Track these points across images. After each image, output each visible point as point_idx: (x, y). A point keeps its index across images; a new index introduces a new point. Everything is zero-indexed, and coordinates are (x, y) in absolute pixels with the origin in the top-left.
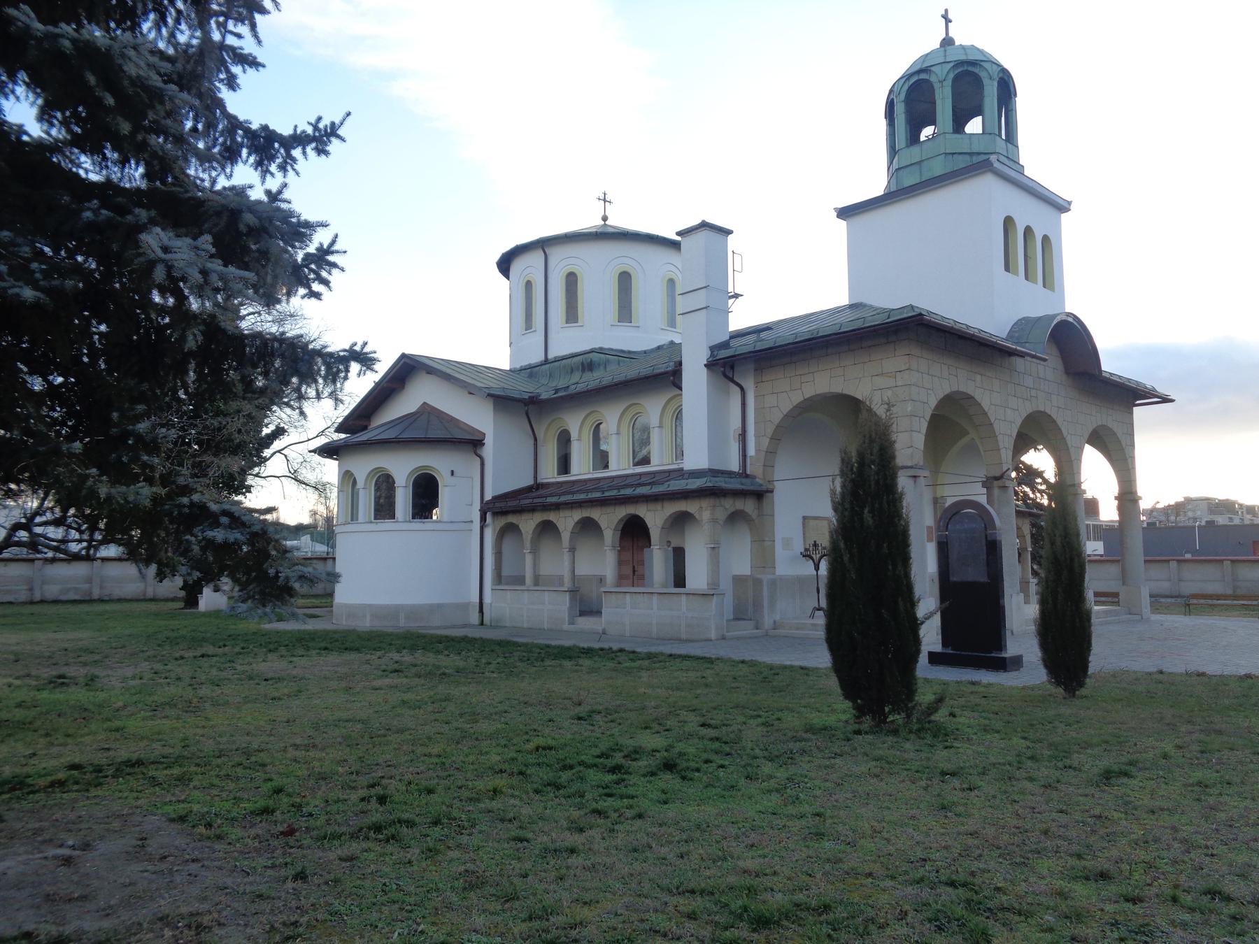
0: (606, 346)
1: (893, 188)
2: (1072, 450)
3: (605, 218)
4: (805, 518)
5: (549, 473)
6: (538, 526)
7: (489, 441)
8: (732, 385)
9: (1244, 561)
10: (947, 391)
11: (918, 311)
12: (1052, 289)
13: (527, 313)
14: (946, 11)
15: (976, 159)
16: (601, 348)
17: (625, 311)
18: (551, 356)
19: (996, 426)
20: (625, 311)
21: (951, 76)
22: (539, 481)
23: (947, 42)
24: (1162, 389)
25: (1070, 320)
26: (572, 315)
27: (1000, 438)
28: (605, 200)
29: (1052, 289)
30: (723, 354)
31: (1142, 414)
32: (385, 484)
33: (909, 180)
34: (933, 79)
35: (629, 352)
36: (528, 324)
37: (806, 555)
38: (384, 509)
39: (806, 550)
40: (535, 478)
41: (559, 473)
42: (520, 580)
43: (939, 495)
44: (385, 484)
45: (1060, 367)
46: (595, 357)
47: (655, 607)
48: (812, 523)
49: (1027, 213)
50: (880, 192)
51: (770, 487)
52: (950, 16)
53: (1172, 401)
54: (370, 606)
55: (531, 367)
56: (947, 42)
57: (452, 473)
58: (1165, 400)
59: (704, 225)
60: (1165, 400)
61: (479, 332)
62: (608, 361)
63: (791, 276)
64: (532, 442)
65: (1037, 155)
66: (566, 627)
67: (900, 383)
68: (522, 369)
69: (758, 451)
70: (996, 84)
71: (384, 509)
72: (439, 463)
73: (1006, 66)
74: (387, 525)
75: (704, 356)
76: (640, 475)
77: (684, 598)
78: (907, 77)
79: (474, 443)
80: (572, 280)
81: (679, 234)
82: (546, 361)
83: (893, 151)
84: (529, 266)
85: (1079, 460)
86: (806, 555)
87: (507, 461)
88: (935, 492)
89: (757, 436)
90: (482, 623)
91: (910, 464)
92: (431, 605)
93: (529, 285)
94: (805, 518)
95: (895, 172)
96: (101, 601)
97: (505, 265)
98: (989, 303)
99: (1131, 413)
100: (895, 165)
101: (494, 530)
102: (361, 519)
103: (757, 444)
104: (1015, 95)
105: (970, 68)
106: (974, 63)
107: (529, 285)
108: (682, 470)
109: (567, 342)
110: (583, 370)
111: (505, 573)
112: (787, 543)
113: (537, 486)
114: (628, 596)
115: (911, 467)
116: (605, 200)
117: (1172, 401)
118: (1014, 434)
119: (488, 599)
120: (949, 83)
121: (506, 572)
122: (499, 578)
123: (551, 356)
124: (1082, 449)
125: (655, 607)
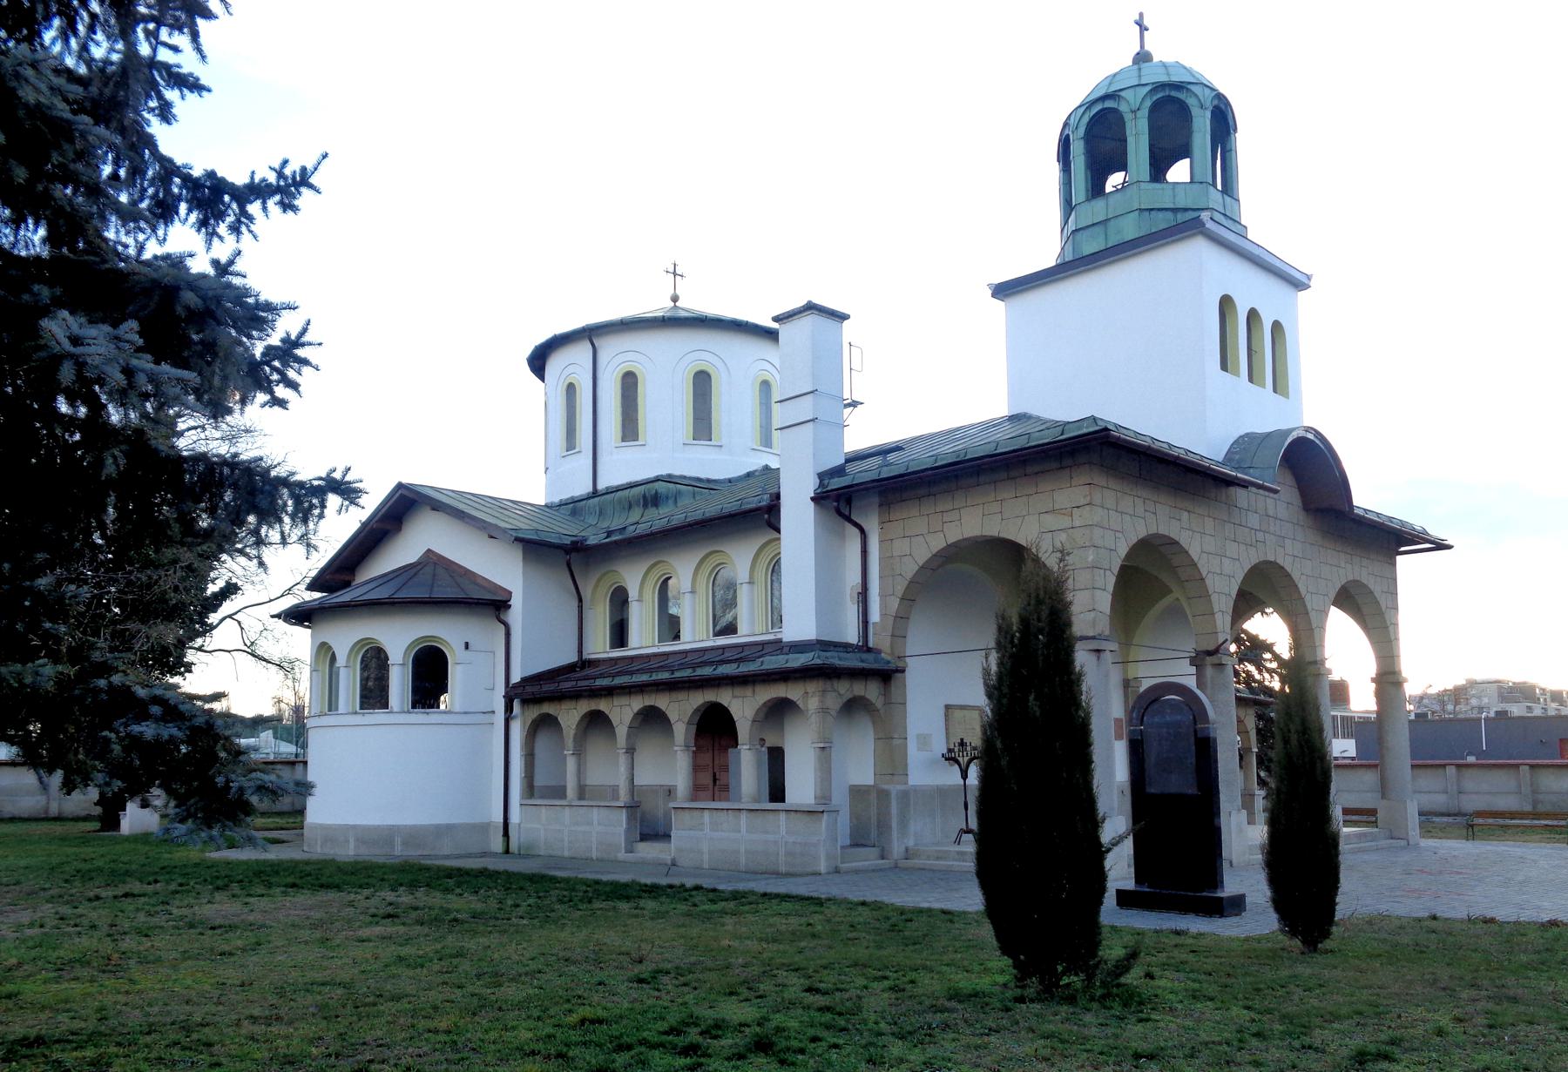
0: (677, 472)
1: (1069, 257)
2: (1313, 615)
4: (948, 707)
5: (599, 646)
6: (585, 716)
7: (516, 602)
11: (1102, 425)
12: (1285, 394)
14: (1141, 15)
15: (1181, 217)
16: (670, 476)
17: (702, 425)
19: (1209, 582)
20: (702, 425)
21: (1148, 103)
23: (1142, 57)
25: (1310, 436)
26: (630, 429)
27: (1214, 598)
28: (675, 274)
29: (1285, 394)
30: (836, 483)
32: (374, 661)
33: (1089, 247)
34: (1123, 108)
35: (709, 481)
37: (950, 758)
38: (374, 695)
40: (580, 652)
42: (559, 792)
43: (1130, 676)
44: (374, 661)
45: (1296, 500)
47: (743, 829)
49: (1251, 291)
50: (1049, 261)
51: (900, 664)
52: (1146, 22)
54: (354, 827)
56: (1142, 57)
57: (467, 646)
58: (1440, 546)
59: (811, 307)
60: (1440, 546)
61: (509, 455)
62: (679, 493)
64: (575, 603)
66: (622, 855)
67: (1077, 523)
70: (1208, 114)
73: (1222, 90)
74: (378, 716)
75: (810, 486)
76: (723, 648)
78: (1088, 104)
79: (495, 605)
80: (629, 382)
81: (776, 319)
82: (595, 493)
84: (571, 364)
85: (1322, 628)
86: (950, 758)
88: (1125, 671)
89: (882, 596)
90: (507, 851)
92: (438, 827)
93: (571, 389)
94: (948, 707)
95: (1072, 236)
97: (538, 362)
99: (1394, 564)
100: (1071, 226)
101: (524, 723)
102: (342, 707)
104: (1235, 130)
105: (1173, 93)
106: (1179, 86)
107: (571, 389)
108: (780, 641)
109: (625, 466)
110: (645, 506)
112: (924, 741)
114: (706, 813)
115: (1093, 638)
116: (675, 274)
117: (1449, 547)
118: (1234, 593)
119: (515, 817)
120: (1145, 112)
121: (539, 781)
122: (530, 789)
123: (601, 486)
125: (743, 829)
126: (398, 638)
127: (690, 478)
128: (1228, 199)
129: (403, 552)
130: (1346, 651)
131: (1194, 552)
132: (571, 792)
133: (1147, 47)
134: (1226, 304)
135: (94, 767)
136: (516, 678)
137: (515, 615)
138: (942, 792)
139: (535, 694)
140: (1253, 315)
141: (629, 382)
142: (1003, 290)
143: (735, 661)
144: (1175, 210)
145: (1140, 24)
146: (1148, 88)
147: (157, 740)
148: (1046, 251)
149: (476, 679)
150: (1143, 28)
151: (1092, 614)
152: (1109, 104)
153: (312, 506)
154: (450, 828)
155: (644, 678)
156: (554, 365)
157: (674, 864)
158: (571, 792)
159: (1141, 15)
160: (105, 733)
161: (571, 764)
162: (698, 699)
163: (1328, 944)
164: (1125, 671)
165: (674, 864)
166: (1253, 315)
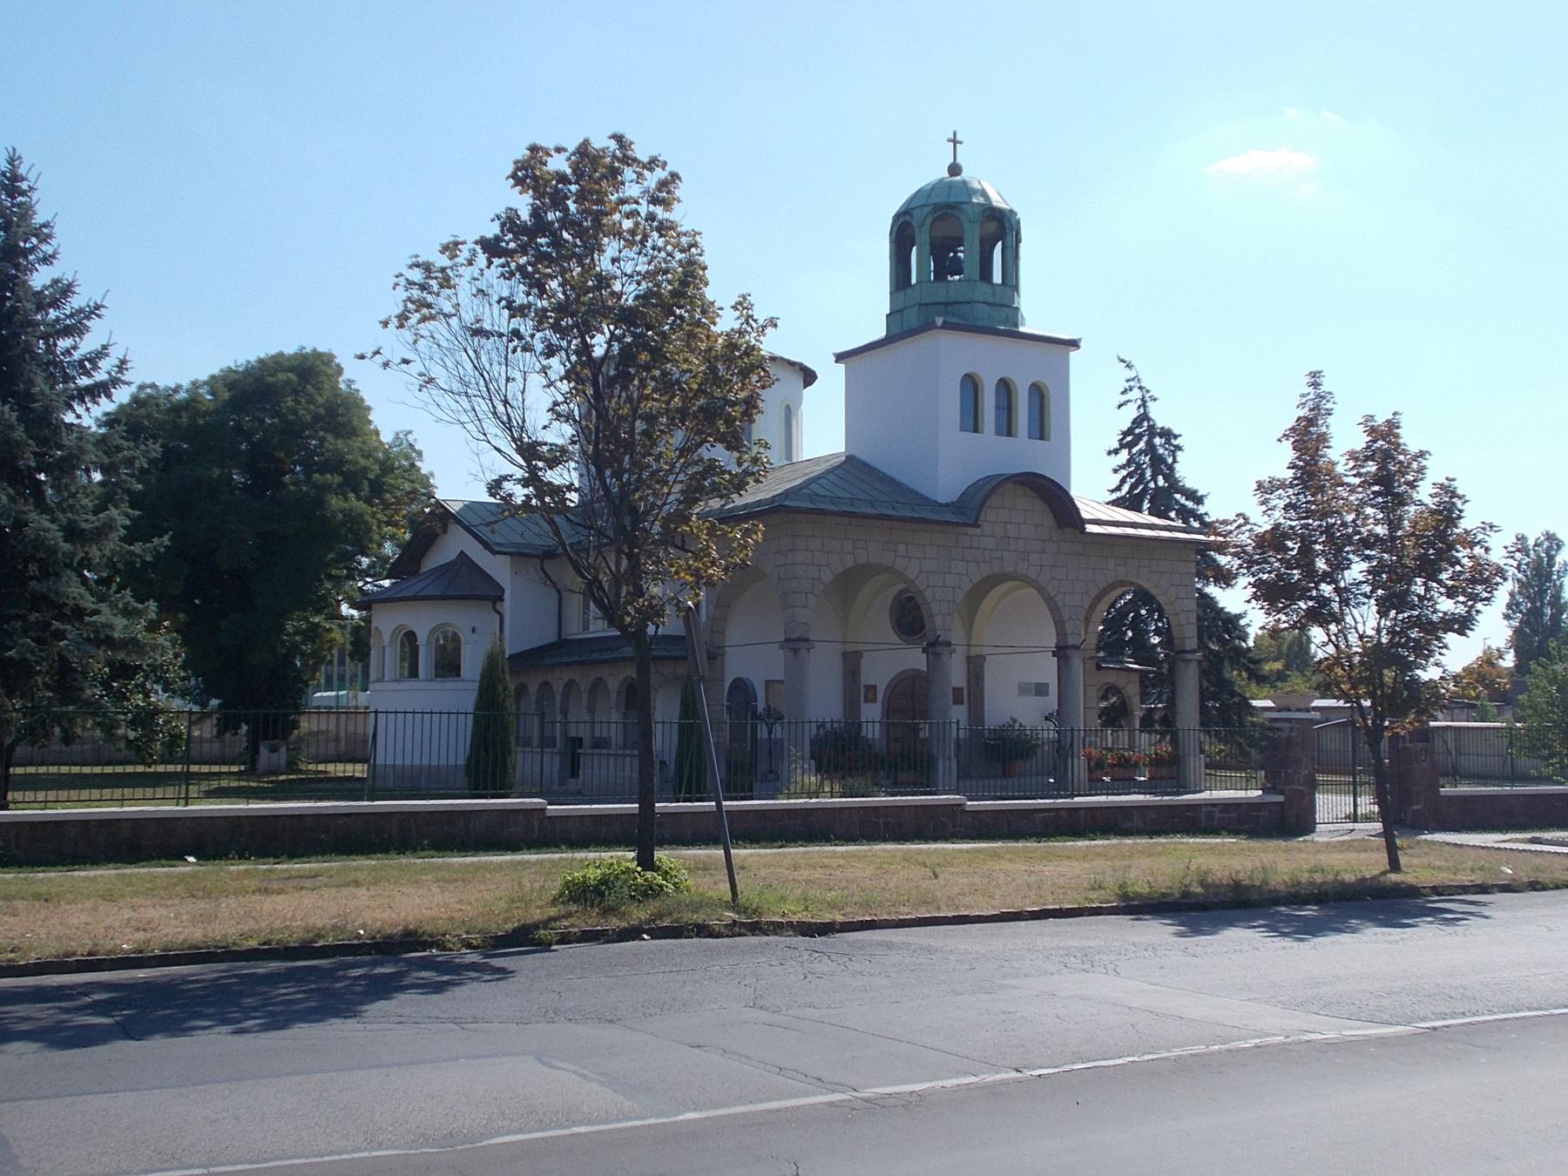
1: (895, 331)
7: (507, 596)
21: (929, 221)
23: (955, 169)
34: (914, 223)
40: (559, 635)
52: (959, 138)
57: (474, 630)
113: (562, 645)
132: (535, 742)
133: (959, 161)
134: (971, 384)
135: (324, 488)
137: (507, 606)
140: (1005, 386)
142: (840, 358)
147: (67, 705)
150: (955, 142)
152: (908, 218)
153: (538, 286)
158: (535, 742)
160: (137, 513)
166: (1005, 386)
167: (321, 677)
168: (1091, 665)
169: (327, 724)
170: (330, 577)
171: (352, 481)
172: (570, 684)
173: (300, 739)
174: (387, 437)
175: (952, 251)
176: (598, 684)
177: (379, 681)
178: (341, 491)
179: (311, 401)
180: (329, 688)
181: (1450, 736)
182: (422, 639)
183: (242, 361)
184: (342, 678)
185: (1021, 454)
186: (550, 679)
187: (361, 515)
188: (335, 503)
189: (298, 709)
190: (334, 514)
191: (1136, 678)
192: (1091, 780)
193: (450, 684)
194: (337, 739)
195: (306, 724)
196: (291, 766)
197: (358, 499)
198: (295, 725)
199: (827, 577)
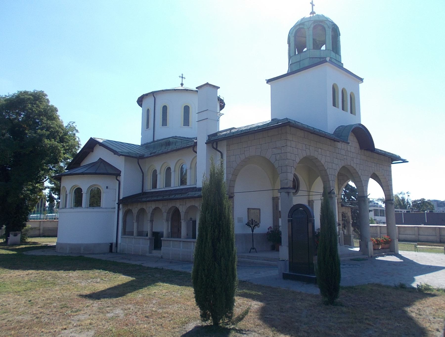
0: (178, 136)
1: (290, 72)
2: (363, 182)
3: (182, 85)
4: (248, 209)
5: (148, 188)
6: (139, 210)
7: (122, 174)
8: (218, 152)
9: (168, 226)
10: (305, 155)
11: (289, 120)
12: (355, 114)
13: (147, 122)
14: (312, 1)
15: (322, 60)
16: (176, 136)
17: (186, 122)
18: (155, 140)
19: (328, 171)
20: (186, 122)
21: (312, 26)
22: (144, 191)
23: (313, 13)
24: (402, 157)
25: (361, 127)
26: (165, 122)
27: (330, 176)
28: (182, 77)
29: (355, 114)
30: (213, 138)
31: (395, 168)
32: (78, 192)
33: (294, 69)
34: (305, 27)
35: (188, 138)
36: (148, 127)
37: (248, 224)
38: (78, 203)
39: (248, 222)
40: (143, 189)
41: (153, 188)
42: (131, 234)
43: (310, 199)
44: (78, 192)
45: (357, 145)
46: (171, 140)
47: (181, 247)
48: (252, 211)
49: (343, 83)
50: (286, 73)
51: (232, 195)
52: (314, 3)
53: (408, 162)
54: (69, 244)
55: (147, 144)
56: (313, 13)
57: (107, 187)
58: (404, 161)
59: (207, 84)
60: (404, 161)
61: (129, 130)
62: (177, 142)
63: (247, 108)
64: (142, 175)
65: (348, 60)
66: (148, 254)
67: (283, 152)
68: (144, 144)
69: (227, 180)
70: (331, 30)
71: (78, 203)
72: (101, 182)
73: (335, 23)
74: (78, 209)
75: (205, 139)
76: (182, 189)
77: (181, 244)
78: (295, 26)
79: (116, 173)
80: (165, 108)
81: (196, 88)
82: (154, 141)
83: (290, 57)
84: (149, 102)
85: (367, 186)
86: (248, 224)
87: (129, 183)
88: (309, 198)
89: (227, 174)
90: (117, 252)
91: (286, 187)
92: (95, 244)
93: (148, 110)
94: (248, 209)
95: (290, 65)
96: (180, 241)
97: (140, 101)
98: (332, 119)
99: (390, 167)
100: (291, 63)
101: (123, 211)
102: (67, 207)
103: (227, 177)
104: (340, 35)
105: (320, 23)
106: (322, 21)
107: (148, 110)
108: (196, 187)
109: (163, 133)
110: (166, 145)
111: (127, 230)
112: (240, 220)
113: (143, 194)
114: (171, 242)
115: (287, 188)
116: (182, 77)
117: (408, 162)
118: (336, 174)
119: (119, 241)
120: (311, 29)
121: (127, 230)
122: (124, 232)
123: (155, 140)
124: (367, 181)
125: (181, 247)
126: (85, 184)
127: (182, 137)
128: (337, 56)
129: (93, 158)
130: (375, 191)
131: (323, 162)
133: (314, 10)
135: (42, 136)
136: (121, 198)
138: (245, 236)
139: (125, 202)
141: (165, 108)
142: (269, 81)
143: (180, 194)
144: (320, 58)
145: (312, 3)
146: (312, 22)
148: (285, 70)
149: (109, 199)
151: (287, 181)
154: (99, 244)
155: (155, 198)
156: (144, 103)
157: (162, 258)
159: (312, 1)
161: (135, 225)
162: (171, 205)
163: (338, 300)
164: (309, 198)
165: (162, 258)
167: (35, 209)
168: (340, 205)
169: (36, 225)
170: (43, 170)
171: (52, 135)
172: (156, 209)
173: (27, 230)
174: (65, 124)
175: (314, 44)
176: (142, 211)
177: (63, 208)
178: (48, 137)
179: (38, 106)
180: (34, 213)
181: (378, 228)
182: (84, 191)
183: (11, 93)
184: (38, 211)
185: (348, 120)
186: (144, 207)
187: (57, 147)
188: (47, 141)
189: (26, 219)
190: (46, 145)
191: (350, 210)
192: (374, 249)
193: (96, 209)
194: (39, 230)
195: (29, 225)
196: (23, 241)
197: (55, 141)
198: (25, 225)
199: (298, 160)
